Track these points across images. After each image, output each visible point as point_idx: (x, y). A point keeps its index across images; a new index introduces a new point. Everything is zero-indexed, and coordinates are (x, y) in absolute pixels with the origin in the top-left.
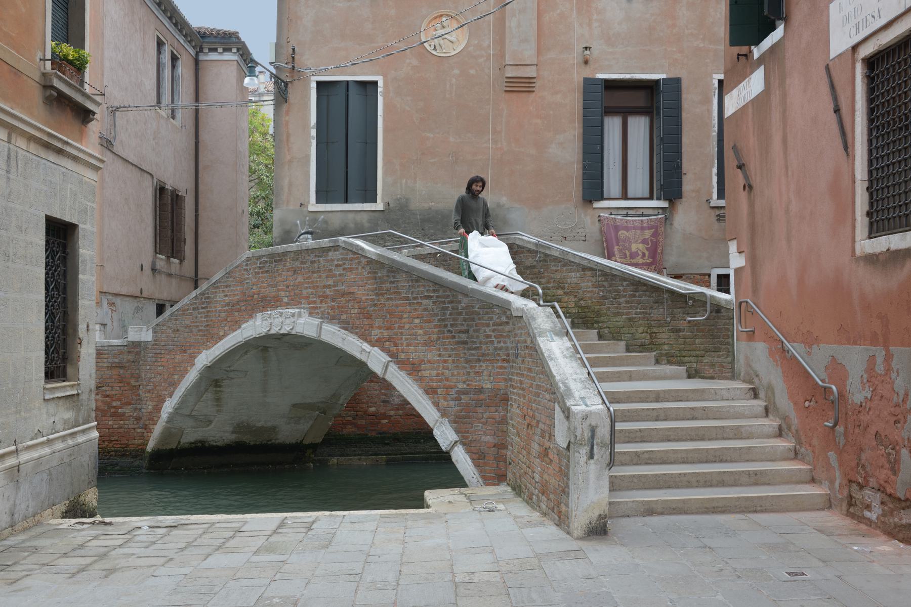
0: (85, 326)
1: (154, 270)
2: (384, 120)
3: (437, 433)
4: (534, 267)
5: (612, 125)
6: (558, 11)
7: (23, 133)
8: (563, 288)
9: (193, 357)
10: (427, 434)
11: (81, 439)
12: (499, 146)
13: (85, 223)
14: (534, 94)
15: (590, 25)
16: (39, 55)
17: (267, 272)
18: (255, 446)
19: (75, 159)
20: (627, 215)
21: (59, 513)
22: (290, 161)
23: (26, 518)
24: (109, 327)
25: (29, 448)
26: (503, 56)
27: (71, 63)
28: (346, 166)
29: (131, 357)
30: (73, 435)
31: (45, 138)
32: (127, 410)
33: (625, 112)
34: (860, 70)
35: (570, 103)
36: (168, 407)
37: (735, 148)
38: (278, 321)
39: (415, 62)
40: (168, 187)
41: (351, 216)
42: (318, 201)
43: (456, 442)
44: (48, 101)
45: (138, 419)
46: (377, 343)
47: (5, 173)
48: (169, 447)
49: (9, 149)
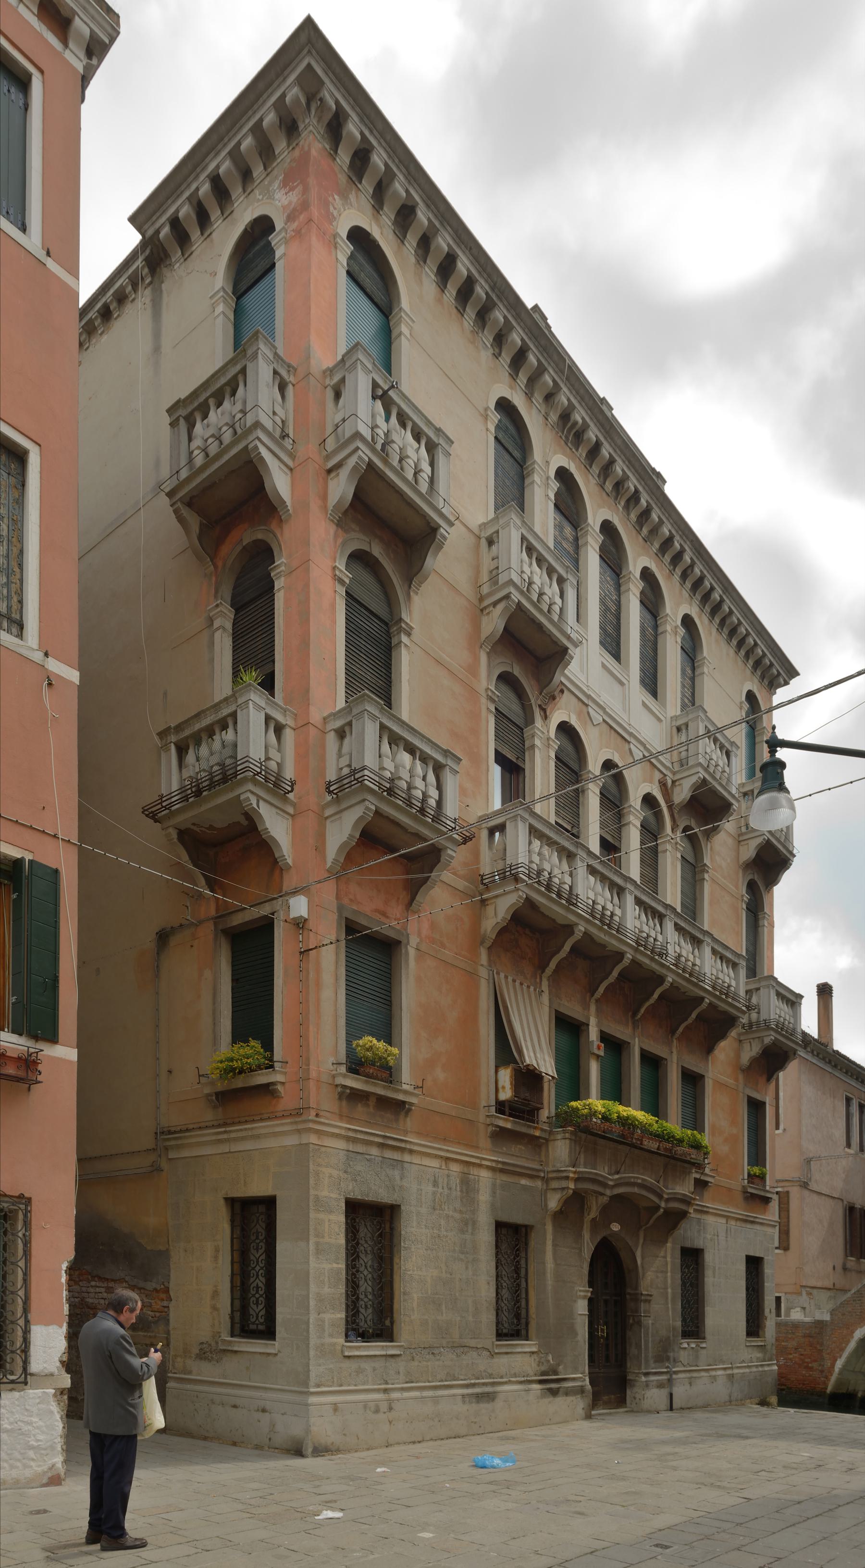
1: (845, 1269)
7: (733, 1218)
9: (853, 1332)
11: (766, 1368)
16: (741, 1177)
19: (761, 1224)
23: (737, 1400)
24: (807, 1310)
25: (738, 1367)
27: (758, 1177)
30: (762, 1366)
32: (815, 1365)
36: (839, 1364)
45: (822, 1371)
48: (841, 1391)
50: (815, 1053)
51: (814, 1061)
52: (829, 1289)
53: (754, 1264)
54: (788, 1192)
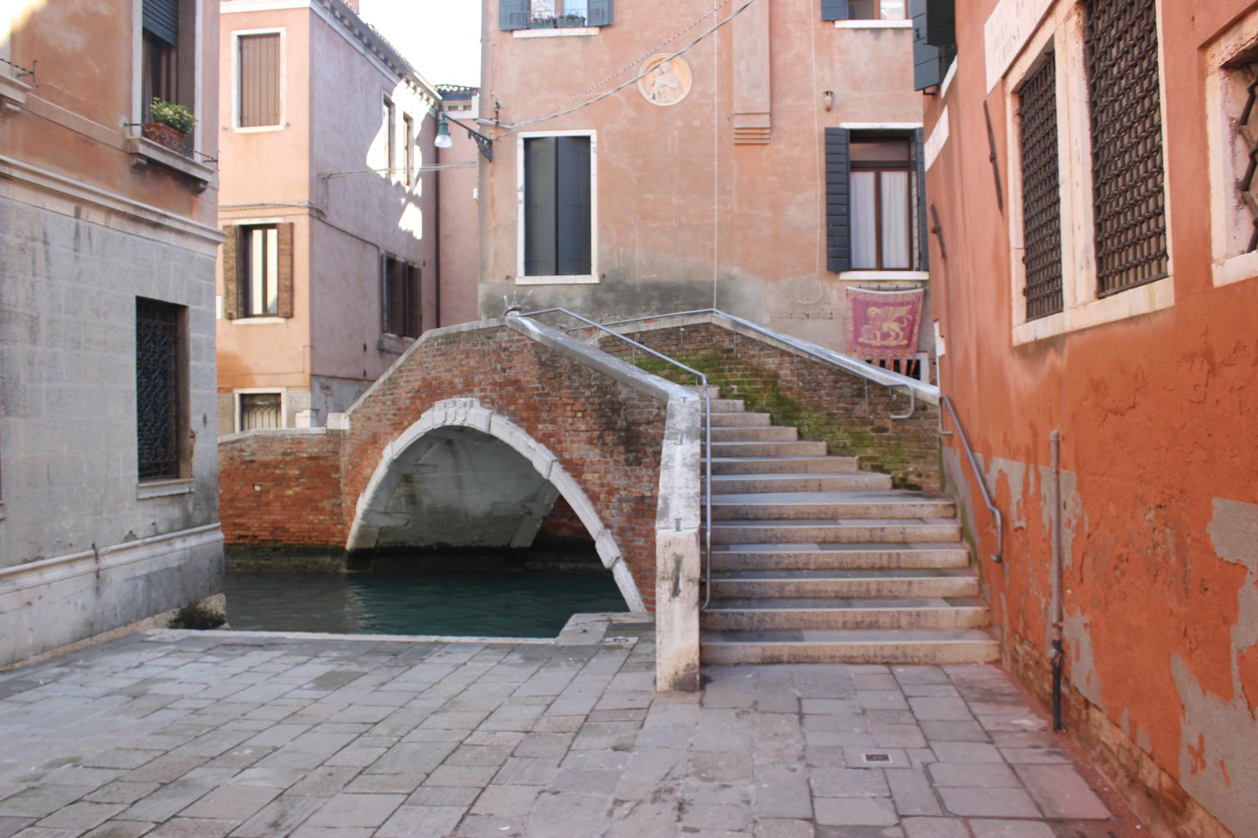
0: (201, 418)
2: (599, 180)
3: (598, 546)
4: (731, 351)
5: (863, 183)
6: (795, 51)
8: (761, 376)
10: (587, 545)
12: (729, 207)
13: (198, 303)
14: (767, 148)
15: (831, 66)
16: (123, 119)
17: (443, 355)
18: (429, 548)
19: (180, 232)
20: (879, 289)
21: (165, 622)
22: (496, 229)
26: (731, 104)
28: (560, 233)
29: (330, 447)
31: (132, 211)
33: (878, 168)
34: (1011, 106)
35: (812, 159)
36: (363, 503)
37: (933, 207)
38: (451, 411)
39: (632, 113)
40: (400, 259)
41: (563, 289)
42: (587, 271)
43: (618, 558)
44: (137, 168)
46: (544, 439)
47: (71, 251)
49: (77, 226)
50: (337, 14)
51: (336, 27)
52: (358, 380)
53: (161, 326)
54: (292, 225)
